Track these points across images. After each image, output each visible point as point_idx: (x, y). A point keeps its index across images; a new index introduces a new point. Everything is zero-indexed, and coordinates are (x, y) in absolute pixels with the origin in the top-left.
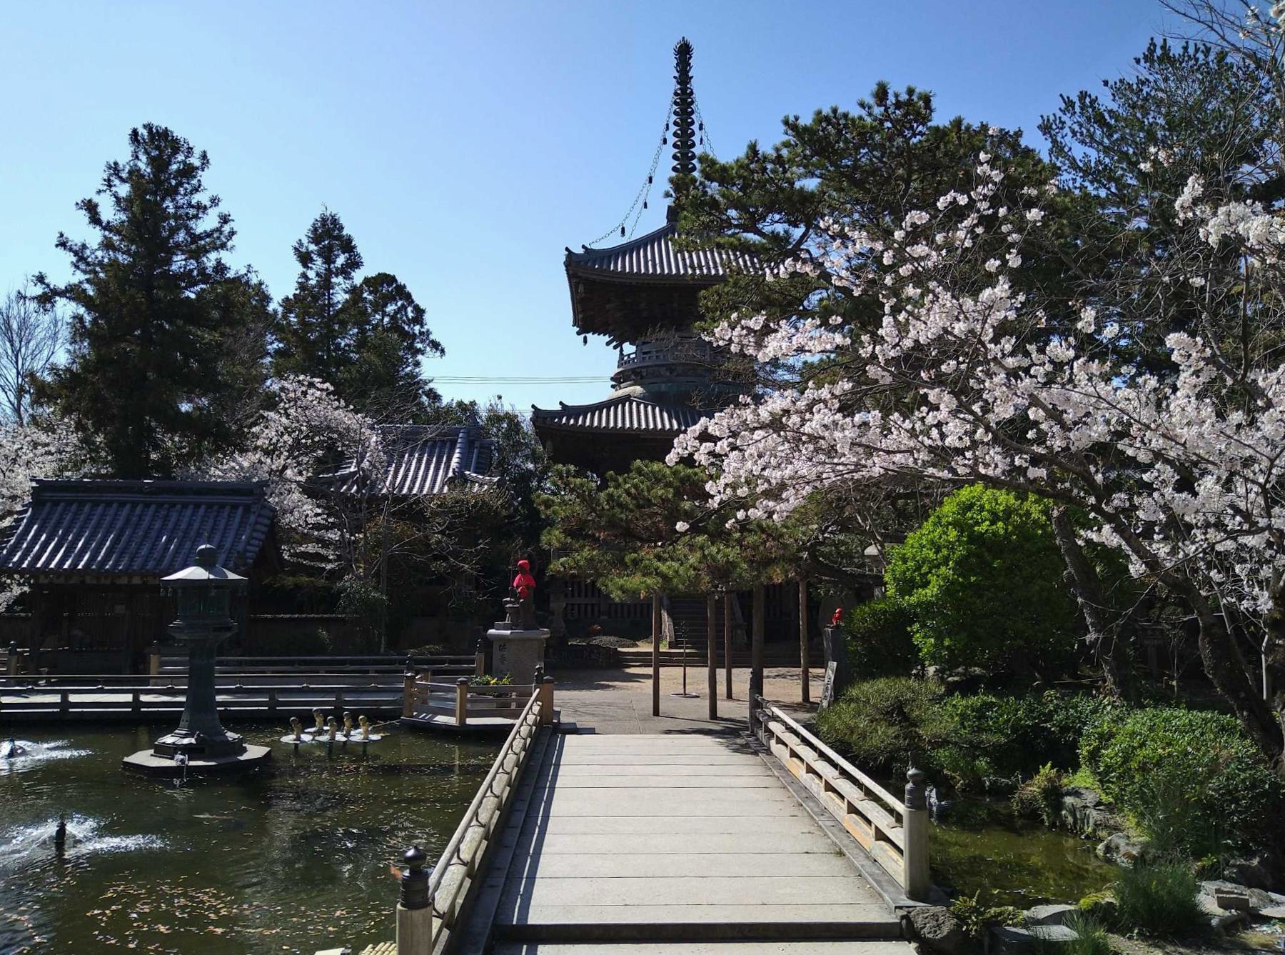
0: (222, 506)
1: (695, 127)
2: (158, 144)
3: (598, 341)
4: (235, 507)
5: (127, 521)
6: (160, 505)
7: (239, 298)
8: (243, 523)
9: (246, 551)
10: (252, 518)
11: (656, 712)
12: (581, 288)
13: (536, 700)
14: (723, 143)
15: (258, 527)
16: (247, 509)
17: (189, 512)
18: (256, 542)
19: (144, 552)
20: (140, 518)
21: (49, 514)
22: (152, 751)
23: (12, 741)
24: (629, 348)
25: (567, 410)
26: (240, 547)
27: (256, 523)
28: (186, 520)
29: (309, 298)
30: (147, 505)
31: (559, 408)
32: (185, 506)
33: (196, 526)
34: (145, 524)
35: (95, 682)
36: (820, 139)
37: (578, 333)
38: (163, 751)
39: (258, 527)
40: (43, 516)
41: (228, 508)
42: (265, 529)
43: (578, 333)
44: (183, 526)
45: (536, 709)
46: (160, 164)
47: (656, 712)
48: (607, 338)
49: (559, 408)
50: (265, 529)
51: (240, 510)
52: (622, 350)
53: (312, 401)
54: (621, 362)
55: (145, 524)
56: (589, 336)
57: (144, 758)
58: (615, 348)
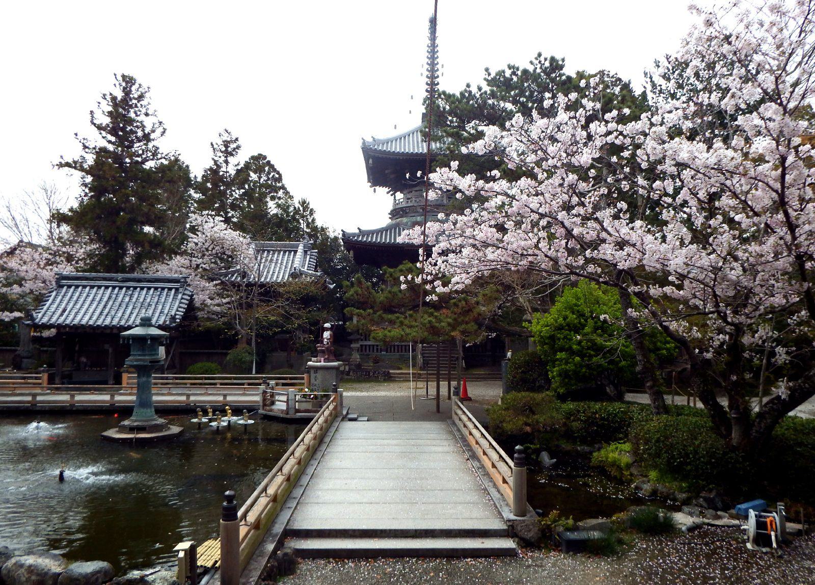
0: (163, 289)
1: (439, 66)
2: (129, 81)
3: (382, 191)
4: (170, 289)
5: (110, 298)
6: (128, 288)
7: (174, 173)
8: (174, 298)
9: (176, 315)
10: (180, 296)
11: (438, 411)
12: (371, 161)
13: (332, 401)
14: (451, 85)
15: (183, 301)
16: (177, 289)
17: (145, 291)
18: (182, 310)
19: (119, 315)
20: (117, 295)
21: (66, 292)
22: (117, 429)
23: (38, 423)
24: (399, 196)
25: (362, 233)
26: (173, 313)
27: (182, 298)
28: (143, 297)
29: (214, 174)
30: (121, 288)
31: (357, 231)
32: (142, 288)
33: (148, 300)
34: (120, 299)
35: (89, 389)
36: (502, 84)
37: (371, 187)
38: (123, 429)
39: (183, 301)
40: (62, 294)
41: (166, 290)
42: (187, 302)
43: (371, 187)
44: (141, 300)
45: (331, 407)
46: (127, 92)
47: (438, 411)
48: (387, 189)
49: (357, 231)
50: (187, 302)
51: (173, 291)
52: (395, 197)
53: (212, 228)
54: (395, 203)
55: (120, 299)
56: (377, 188)
57: (113, 433)
58: (392, 195)
